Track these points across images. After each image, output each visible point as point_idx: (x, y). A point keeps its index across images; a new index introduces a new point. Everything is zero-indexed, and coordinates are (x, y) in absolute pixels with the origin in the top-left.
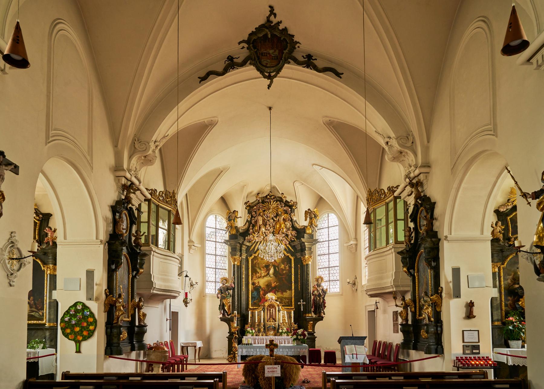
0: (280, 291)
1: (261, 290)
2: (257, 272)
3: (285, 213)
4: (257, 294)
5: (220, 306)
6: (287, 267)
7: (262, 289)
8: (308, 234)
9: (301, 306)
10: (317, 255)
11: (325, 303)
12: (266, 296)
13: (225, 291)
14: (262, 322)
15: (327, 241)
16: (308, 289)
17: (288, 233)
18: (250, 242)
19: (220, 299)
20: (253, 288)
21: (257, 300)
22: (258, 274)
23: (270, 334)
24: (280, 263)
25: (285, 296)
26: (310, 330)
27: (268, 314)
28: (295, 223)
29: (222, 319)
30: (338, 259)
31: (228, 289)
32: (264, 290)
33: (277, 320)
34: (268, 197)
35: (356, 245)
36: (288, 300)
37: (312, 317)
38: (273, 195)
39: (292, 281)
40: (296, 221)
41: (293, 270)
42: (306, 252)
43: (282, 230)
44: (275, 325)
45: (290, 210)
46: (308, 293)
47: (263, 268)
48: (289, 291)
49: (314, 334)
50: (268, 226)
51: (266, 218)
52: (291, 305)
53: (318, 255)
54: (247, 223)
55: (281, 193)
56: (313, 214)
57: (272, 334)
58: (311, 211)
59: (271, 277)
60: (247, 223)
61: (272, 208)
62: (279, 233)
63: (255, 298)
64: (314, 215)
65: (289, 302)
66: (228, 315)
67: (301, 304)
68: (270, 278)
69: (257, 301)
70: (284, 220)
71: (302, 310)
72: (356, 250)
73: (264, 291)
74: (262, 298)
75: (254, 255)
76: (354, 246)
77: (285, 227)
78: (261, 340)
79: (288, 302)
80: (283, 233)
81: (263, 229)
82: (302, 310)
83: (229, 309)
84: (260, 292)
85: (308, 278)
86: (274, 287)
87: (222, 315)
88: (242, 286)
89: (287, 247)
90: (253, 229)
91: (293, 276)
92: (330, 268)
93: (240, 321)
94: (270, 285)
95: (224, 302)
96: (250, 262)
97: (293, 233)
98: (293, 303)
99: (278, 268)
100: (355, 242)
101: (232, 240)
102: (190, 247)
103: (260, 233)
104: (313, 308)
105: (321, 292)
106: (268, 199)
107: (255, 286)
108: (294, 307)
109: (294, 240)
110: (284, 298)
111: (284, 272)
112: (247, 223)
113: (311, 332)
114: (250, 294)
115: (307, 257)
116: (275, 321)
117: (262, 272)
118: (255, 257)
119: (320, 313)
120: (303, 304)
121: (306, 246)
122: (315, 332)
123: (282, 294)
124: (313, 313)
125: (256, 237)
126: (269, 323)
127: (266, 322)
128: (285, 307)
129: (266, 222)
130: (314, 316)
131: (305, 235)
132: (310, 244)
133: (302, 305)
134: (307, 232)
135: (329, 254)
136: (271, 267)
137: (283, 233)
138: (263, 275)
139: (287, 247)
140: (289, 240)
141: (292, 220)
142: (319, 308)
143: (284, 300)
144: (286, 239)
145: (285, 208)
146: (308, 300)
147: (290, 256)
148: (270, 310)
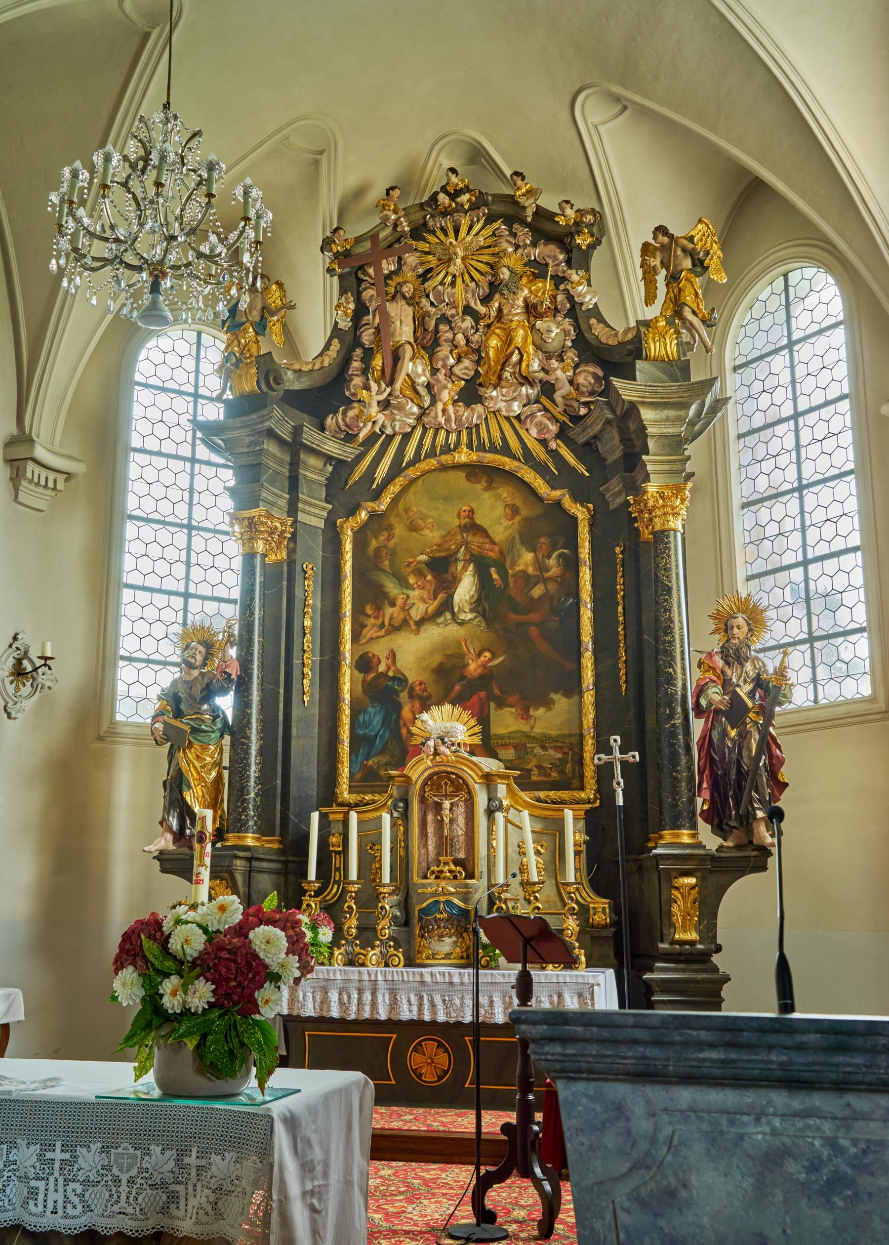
1: (404, 696)
2: (385, 595)
3: (535, 276)
4: (385, 722)
6: (552, 562)
8: (655, 359)
10: (736, 502)
11: (781, 762)
14: (312, 875)
15: (787, 419)
16: (670, 680)
17: (551, 378)
18: (349, 438)
20: (359, 688)
21: (381, 752)
22: (389, 611)
23: (433, 956)
24: (511, 542)
26: (685, 929)
27: (431, 830)
28: (593, 321)
30: (852, 505)
33: (481, 866)
34: (443, 199)
36: (556, 748)
37: (700, 846)
38: (467, 189)
39: (579, 642)
40: (595, 312)
41: (586, 575)
42: (652, 462)
43: (515, 358)
44: (466, 898)
45: (561, 257)
46: (670, 704)
47: (419, 573)
49: (716, 959)
50: (444, 350)
53: (745, 506)
54: (336, 342)
55: (508, 172)
56: (684, 250)
57: (448, 956)
58: (671, 237)
59: (462, 623)
60: (336, 345)
61: (460, 253)
63: (369, 741)
64: (691, 254)
67: (610, 765)
69: (384, 759)
71: (620, 801)
75: (370, 505)
77: (538, 347)
78: (360, 992)
79: (559, 766)
80: (526, 380)
82: (620, 801)
85: (669, 610)
86: (481, 677)
87: (169, 837)
88: (296, 673)
89: (551, 452)
91: (586, 614)
92: (811, 567)
94: (454, 667)
96: (348, 546)
97: (581, 379)
99: (503, 573)
104: (706, 794)
105: (751, 695)
108: (598, 791)
111: (537, 591)
112: (336, 342)
113: (692, 943)
114: (347, 728)
115: (652, 488)
116: (471, 876)
117: (415, 594)
118: (373, 516)
119: (747, 820)
120: (624, 764)
121: (650, 430)
122: (719, 949)
123: (525, 715)
124: (704, 828)
126: (431, 885)
128: (542, 794)
129: (436, 330)
130: (711, 841)
131: (639, 364)
132: (672, 413)
133: (618, 772)
134: (654, 348)
135: (801, 488)
136: (460, 566)
137: (526, 380)
138: (416, 614)
139: (551, 452)
140: (557, 411)
142: (740, 789)
143: (538, 750)
144: (546, 409)
145: (536, 253)
146: (673, 745)
147: (568, 503)
148: (438, 807)
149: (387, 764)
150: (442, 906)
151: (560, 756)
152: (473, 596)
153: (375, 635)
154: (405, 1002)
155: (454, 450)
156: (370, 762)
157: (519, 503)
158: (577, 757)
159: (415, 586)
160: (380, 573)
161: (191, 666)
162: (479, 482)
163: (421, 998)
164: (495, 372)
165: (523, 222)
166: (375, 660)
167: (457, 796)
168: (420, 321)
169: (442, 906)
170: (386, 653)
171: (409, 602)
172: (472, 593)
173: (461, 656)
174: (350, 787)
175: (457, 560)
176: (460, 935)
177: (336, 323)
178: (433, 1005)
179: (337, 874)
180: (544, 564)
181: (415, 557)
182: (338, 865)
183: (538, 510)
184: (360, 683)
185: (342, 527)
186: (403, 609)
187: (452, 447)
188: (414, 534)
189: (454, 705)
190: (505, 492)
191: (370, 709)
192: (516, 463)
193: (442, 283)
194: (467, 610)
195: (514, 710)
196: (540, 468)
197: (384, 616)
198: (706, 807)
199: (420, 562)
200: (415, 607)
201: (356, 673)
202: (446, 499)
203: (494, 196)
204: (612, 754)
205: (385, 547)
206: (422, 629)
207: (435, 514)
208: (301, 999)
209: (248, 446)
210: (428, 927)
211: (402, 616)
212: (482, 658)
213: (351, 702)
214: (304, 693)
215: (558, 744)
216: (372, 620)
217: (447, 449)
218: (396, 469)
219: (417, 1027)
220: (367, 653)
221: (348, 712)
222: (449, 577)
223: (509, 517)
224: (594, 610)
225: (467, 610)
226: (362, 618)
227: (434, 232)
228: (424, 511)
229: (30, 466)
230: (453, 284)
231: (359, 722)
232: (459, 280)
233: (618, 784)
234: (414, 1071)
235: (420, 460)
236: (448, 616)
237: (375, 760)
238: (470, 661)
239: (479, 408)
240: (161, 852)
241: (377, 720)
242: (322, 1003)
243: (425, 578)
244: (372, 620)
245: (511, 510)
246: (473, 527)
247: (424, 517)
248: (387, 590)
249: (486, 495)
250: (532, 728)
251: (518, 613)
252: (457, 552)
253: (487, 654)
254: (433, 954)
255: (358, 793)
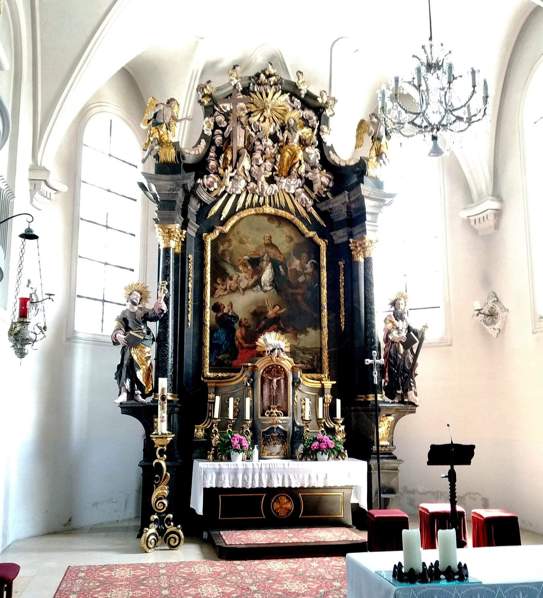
0: (290, 330)
1: (236, 325)
2: (227, 274)
4: (227, 338)
5: (120, 367)
6: (308, 265)
7: (241, 322)
9: (372, 370)
12: (261, 341)
13: (138, 323)
19: (119, 348)
21: (225, 352)
23: (271, 454)
24: (289, 254)
25: (301, 345)
29: (126, 409)
31: (147, 318)
32: (245, 327)
34: (262, 76)
35: (498, 213)
36: (310, 354)
40: (331, 148)
43: (297, 166)
47: (245, 265)
48: (313, 331)
50: (257, 155)
51: (253, 134)
52: (318, 370)
54: (203, 141)
57: (278, 454)
59: (265, 291)
62: (289, 174)
65: (313, 360)
66: (144, 396)
68: (261, 293)
69: (227, 356)
70: (303, 143)
72: (497, 227)
73: (247, 328)
74: (239, 348)
76: (491, 218)
77: (305, 161)
79: (311, 362)
80: (300, 177)
81: (246, 163)
83: (148, 376)
84: (234, 331)
86: (275, 318)
90: (217, 158)
91: (324, 291)
93: (178, 413)
95: (135, 357)
96: (209, 248)
98: (326, 364)
100: (496, 205)
101: (164, 177)
102: (35, 183)
103: (240, 169)
104: (387, 379)
106: (259, 85)
107: (220, 314)
109: (327, 198)
110: (299, 349)
113: (386, 446)
117: (242, 275)
118: (222, 234)
125: (228, 179)
127: (260, 417)
136: (265, 263)
138: (243, 285)
141: (321, 146)
143: (301, 354)
144: (306, 192)
148: (271, 381)
149: (228, 358)
150: (275, 429)
151: (311, 358)
152: (271, 278)
153: (222, 294)
154: (276, 477)
155: (262, 205)
156: (220, 357)
157: (293, 235)
158: (319, 358)
159: (242, 271)
160: (224, 263)
161: (134, 304)
162: (274, 223)
163: (284, 476)
164: (286, 170)
165: (299, 98)
166: (222, 306)
167: (279, 376)
168: (248, 138)
169: (275, 429)
170: (228, 304)
171: (239, 279)
172: (270, 277)
173: (266, 307)
174: (209, 369)
175: (263, 260)
176: (283, 443)
177: (203, 131)
178: (289, 479)
179: (210, 413)
180: (304, 266)
181: (242, 256)
182: (210, 409)
183: (302, 240)
184: (214, 318)
185: (206, 237)
186: (236, 282)
187: (261, 204)
188: (242, 245)
189: (277, 332)
190: (287, 230)
191: (219, 331)
192: (293, 216)
193: (259, 121)
194: (268, 285)
195: (290, 335)
196: (303, 219)
197: (226, 284)
198: (386, 384)
199: (245, 260)
200: (242, 281)
201: (213, 312)
202: (258, 230)
203: (286, 81)
204: (372, 359)
205: (227, 250)
206: (246, 292)
207: (252, 236)
208: (223, 479)
209: (169, 191)
210: (268, 440)
211: (236, 286)
212: (275, 309)
213: (210, 327)
214: (188, 321)
215: (311, 352)
216: (221, 286)
217: (258, 205)
218: (233, 212)
219: (281, 490)
220: (218, 302)
221: (209, 331)
222: (259, 268)
223: (288, 242)
224: (327, 290)
225: (268, 285)
226: (215, 285)
227: (255, 93)
228: (247, 234)
229: (43, 185)
230: (264, 121)
231: (214, 337)
232: (267, 120)
233: (375, 374)
234: (275, 511)
235: (245, 209)
236: (259, 287)
237: (222, 356)
238: (269, 310)
239: (275, 186)
240: (121, 403)
241: (223, 337)
242: (233, 480)
243: (247, 267)
244: (221, 286)
245: (290, 238)
246: (271, 245)
247: (247, 238)
248: (228, 272)
249: (278, 230)
250: (299, 344)
251: (292, 289)
252: (263, 257)
253: (278, 307)
254: (271, 453)
255: (214, 372)
